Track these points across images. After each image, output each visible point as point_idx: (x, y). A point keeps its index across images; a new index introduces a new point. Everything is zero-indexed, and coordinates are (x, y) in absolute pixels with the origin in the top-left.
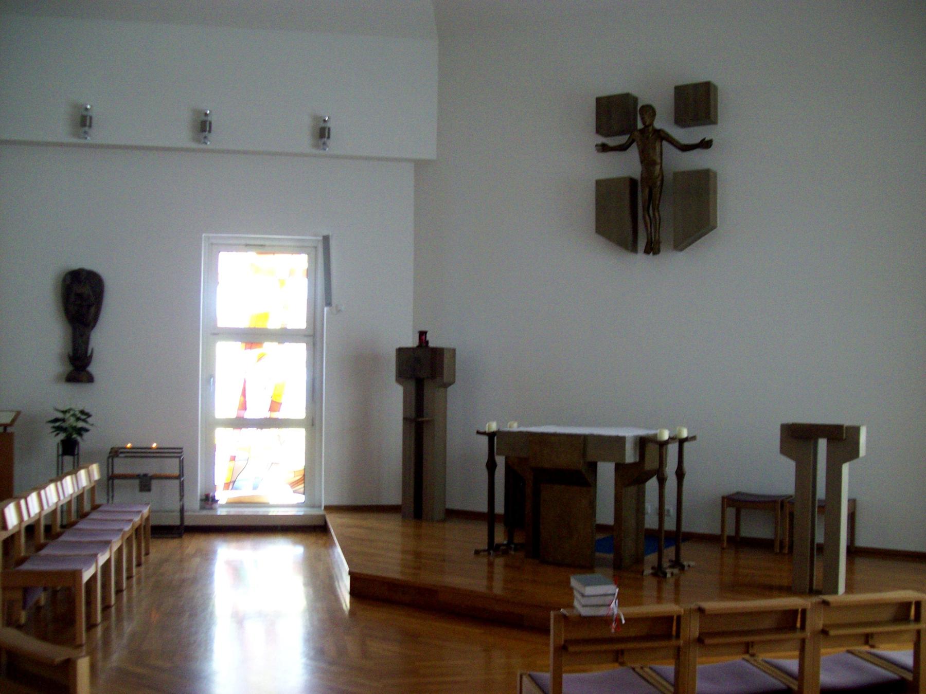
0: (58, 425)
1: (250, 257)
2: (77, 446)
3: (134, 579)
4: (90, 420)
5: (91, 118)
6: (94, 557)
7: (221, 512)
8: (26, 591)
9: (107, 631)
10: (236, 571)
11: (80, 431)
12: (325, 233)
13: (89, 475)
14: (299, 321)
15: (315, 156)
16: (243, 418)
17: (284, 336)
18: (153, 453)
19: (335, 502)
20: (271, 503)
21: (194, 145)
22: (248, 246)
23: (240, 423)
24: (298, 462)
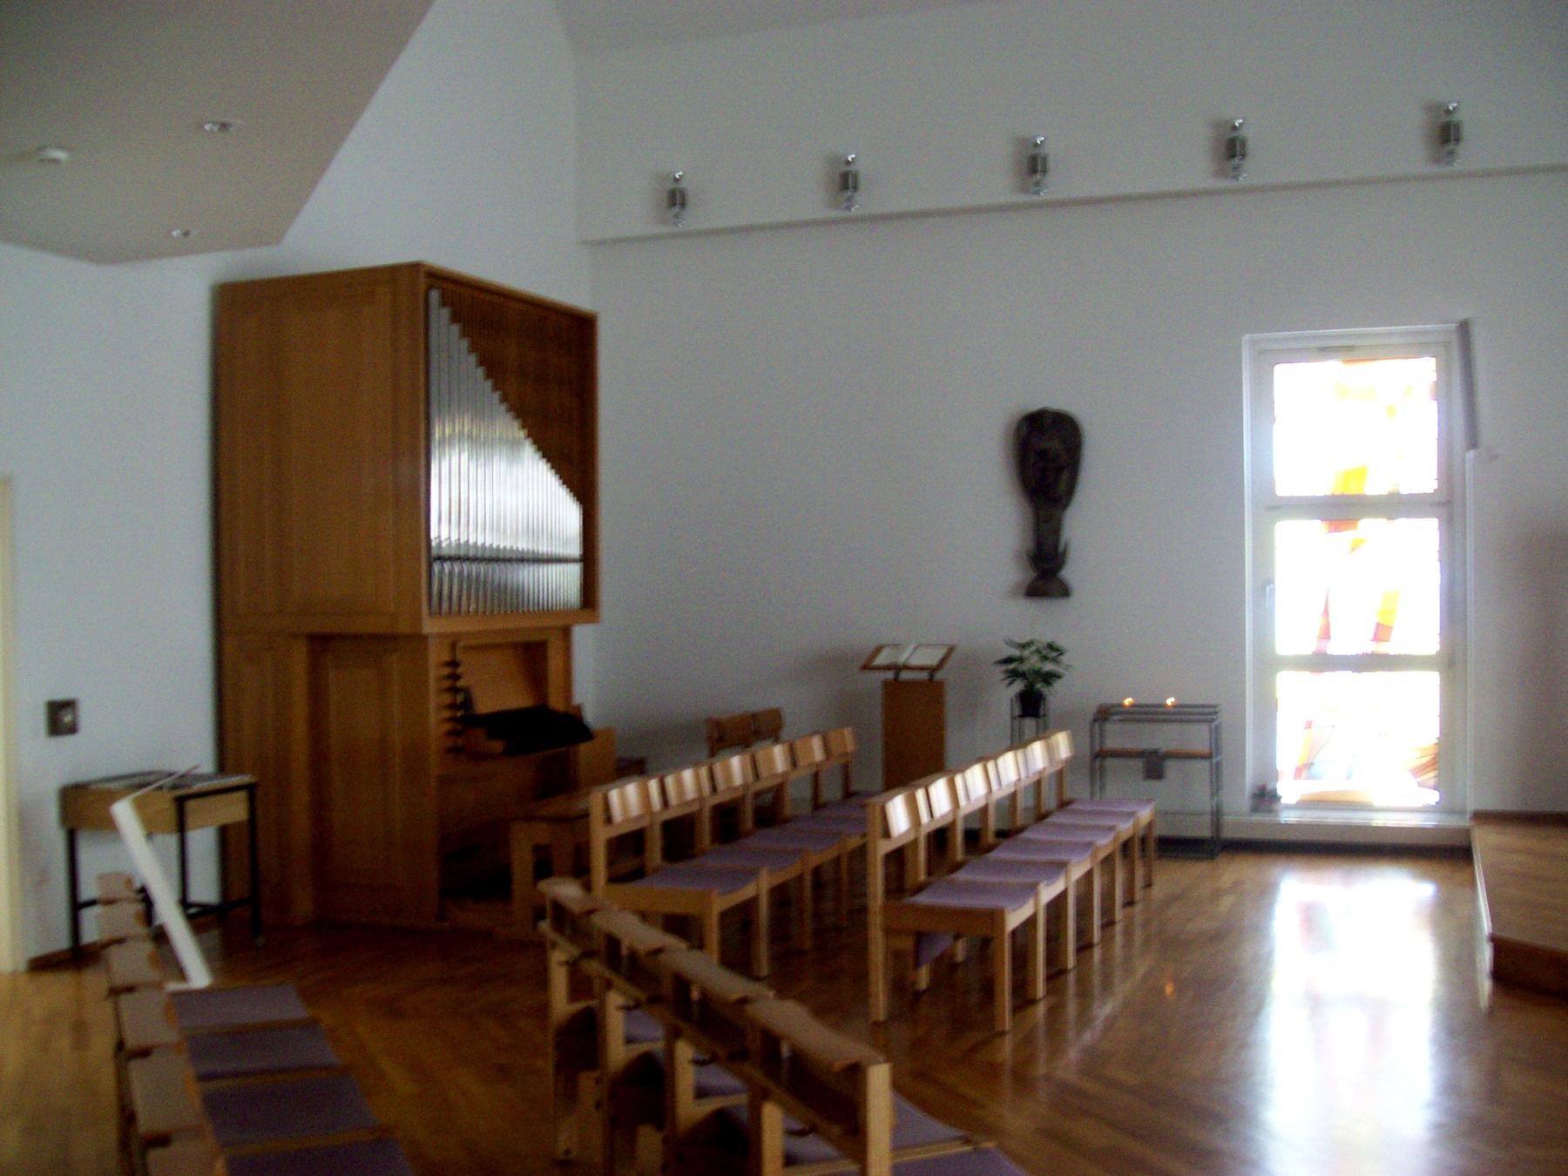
0: (1012, 667)
1: (1331, 370)
2: (1042, 702)
3: (1118, 928)
4: (1064, 658)
5: (1044, 159)
6: (1032, 889)
7: (1288, 817)
8: (920, 938)
9: (1055, 1012)
10: (1310, 918)
11: (1049, 678)
12: (1463, 314)
13: (1050, 752)
14: (1425, 480)
15: (834, 222)
16: (1326, 655)
17: (1395, 506)
18: (1169, 713)
19: (1490, 804)
20: (1377, 804)
21: (1022, 198)
22: (1326, 351)
23: (1321, 662)
24: (1427, 731)
